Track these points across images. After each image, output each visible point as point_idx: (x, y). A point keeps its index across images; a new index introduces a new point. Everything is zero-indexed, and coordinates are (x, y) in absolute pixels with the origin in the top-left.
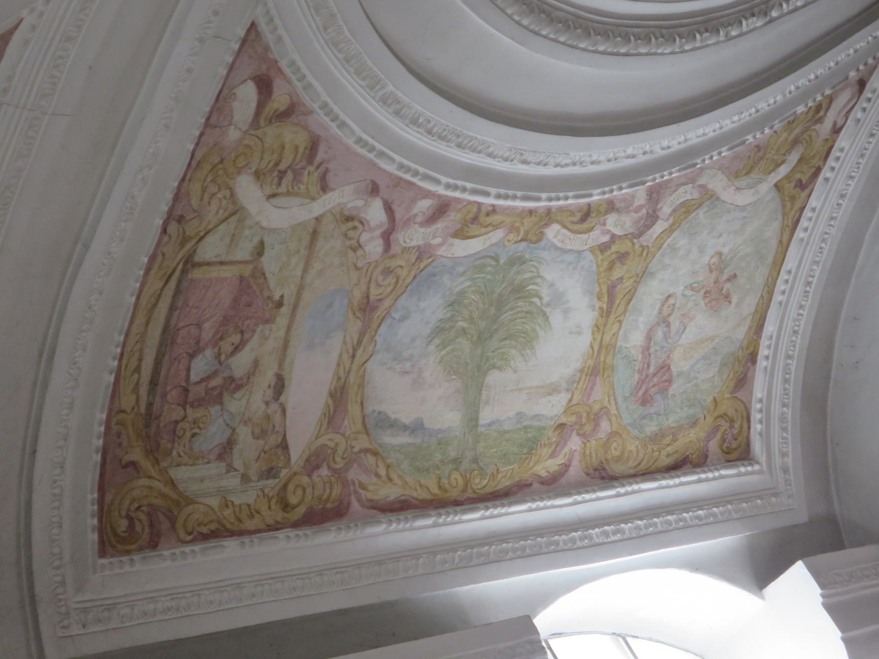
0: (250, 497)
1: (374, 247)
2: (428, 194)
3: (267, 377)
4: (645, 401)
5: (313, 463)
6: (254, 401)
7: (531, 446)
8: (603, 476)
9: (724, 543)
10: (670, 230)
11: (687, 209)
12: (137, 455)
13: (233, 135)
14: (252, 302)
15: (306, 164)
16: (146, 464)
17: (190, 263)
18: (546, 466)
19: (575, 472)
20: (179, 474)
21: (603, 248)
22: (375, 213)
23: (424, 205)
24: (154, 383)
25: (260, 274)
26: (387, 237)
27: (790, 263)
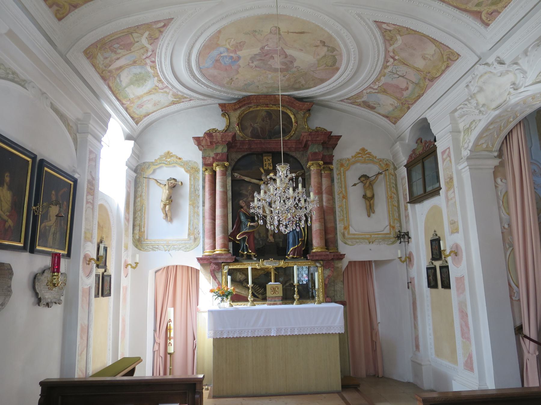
0: (101, 66)
1: (144, 57)
2: (155, 59)
3: (118, 56)
4: (138, 107)
5: (110, 72)
6: (114, 56)
7: (125, 98)
8: (126, 109)
9: (127, 130)
10: (162, 92)
11: (166, 92)
12: (99, 46)
13: (154, 26)
14: (128, 47)
15: (153, 39)
16: (98, 49)
17: (131, 33)
18: (124, 102)
19: (125, 106)
20: (99, 54)
21: (156, 86)
22: (149, 54)
23: (153, 59)
24: (111, 41)
25: (134, 44)
26: (147, 57)
27: (163, 110)
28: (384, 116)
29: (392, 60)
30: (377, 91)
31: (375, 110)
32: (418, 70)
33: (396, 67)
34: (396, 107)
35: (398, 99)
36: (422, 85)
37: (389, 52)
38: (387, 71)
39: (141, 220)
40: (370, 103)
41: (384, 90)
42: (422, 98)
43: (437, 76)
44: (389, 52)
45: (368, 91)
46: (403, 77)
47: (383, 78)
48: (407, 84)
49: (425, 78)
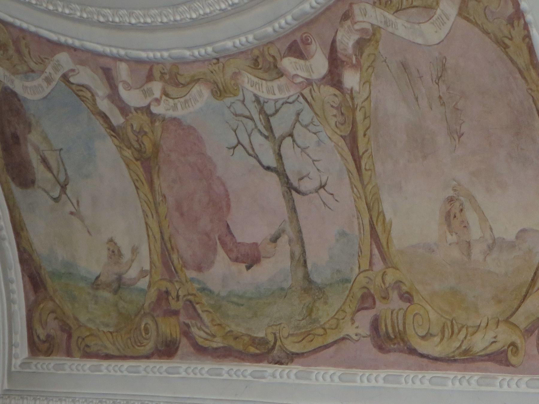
28: (26, 258)
29: (319, 65)
30: (117, 119)
31: (17, 191)
32: (376, 233)
33: (307, 116)
34: (119, 285)
35: (166, 253)
36: (325, 313)
37: (347, 16)
38: (252, 85)
39: (20, 216)
40: (34, 137)
41: (147, 154)
42: (269, 369)
43: (423, 347)
44: (347, 16)
45: (85, 76)
46: (290, 188)
47: (201, 94)
48: (275, 239)
49: (367, 300)
